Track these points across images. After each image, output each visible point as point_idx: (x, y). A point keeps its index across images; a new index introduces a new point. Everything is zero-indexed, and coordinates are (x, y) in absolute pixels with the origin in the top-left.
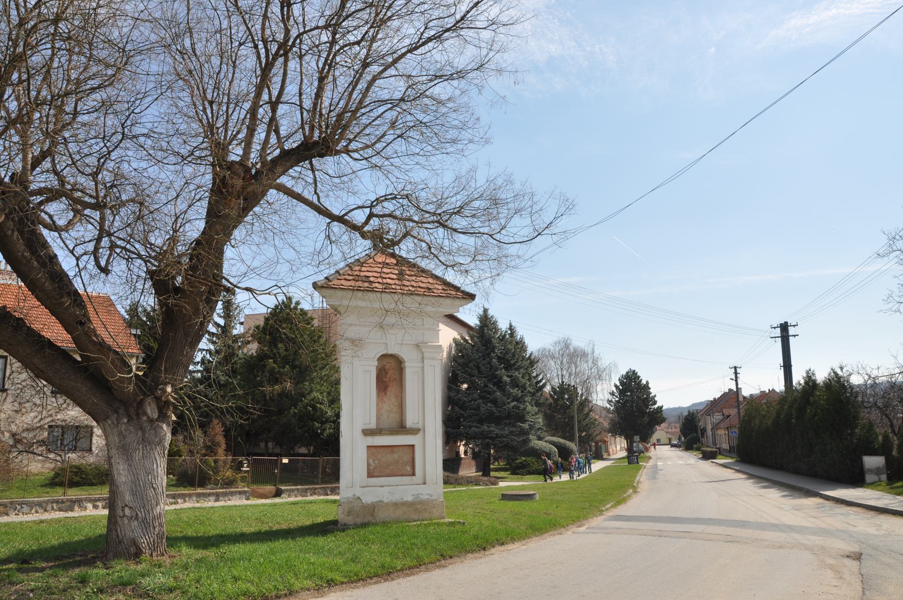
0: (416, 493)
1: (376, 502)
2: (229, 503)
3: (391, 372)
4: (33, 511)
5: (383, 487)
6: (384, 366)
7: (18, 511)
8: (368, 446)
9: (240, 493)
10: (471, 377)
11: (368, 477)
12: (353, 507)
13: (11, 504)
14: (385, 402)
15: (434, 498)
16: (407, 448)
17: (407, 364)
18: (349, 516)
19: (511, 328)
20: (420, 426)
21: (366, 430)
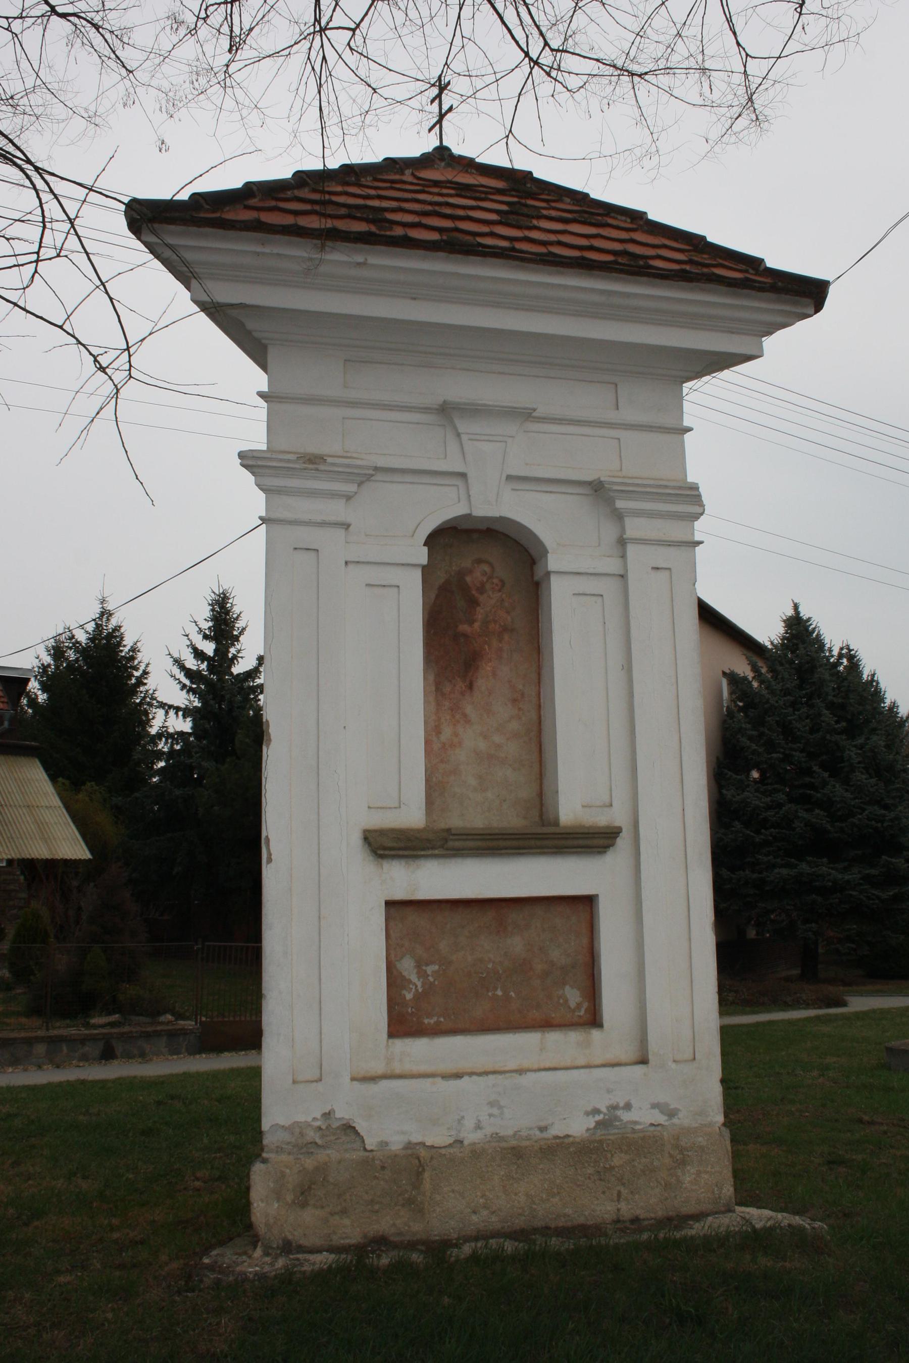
3: (489, 601)
5: (458, 1076)
6: (461, 574)
8: (389, 904)
10: (176, 1020)
11: (392, 1034)
12: (322, 1169)
14: (467, 720)
17: (554, 562)
18: (304, 1205)
19: (134, 649)
20: (618, 816)
21: (382, 832)
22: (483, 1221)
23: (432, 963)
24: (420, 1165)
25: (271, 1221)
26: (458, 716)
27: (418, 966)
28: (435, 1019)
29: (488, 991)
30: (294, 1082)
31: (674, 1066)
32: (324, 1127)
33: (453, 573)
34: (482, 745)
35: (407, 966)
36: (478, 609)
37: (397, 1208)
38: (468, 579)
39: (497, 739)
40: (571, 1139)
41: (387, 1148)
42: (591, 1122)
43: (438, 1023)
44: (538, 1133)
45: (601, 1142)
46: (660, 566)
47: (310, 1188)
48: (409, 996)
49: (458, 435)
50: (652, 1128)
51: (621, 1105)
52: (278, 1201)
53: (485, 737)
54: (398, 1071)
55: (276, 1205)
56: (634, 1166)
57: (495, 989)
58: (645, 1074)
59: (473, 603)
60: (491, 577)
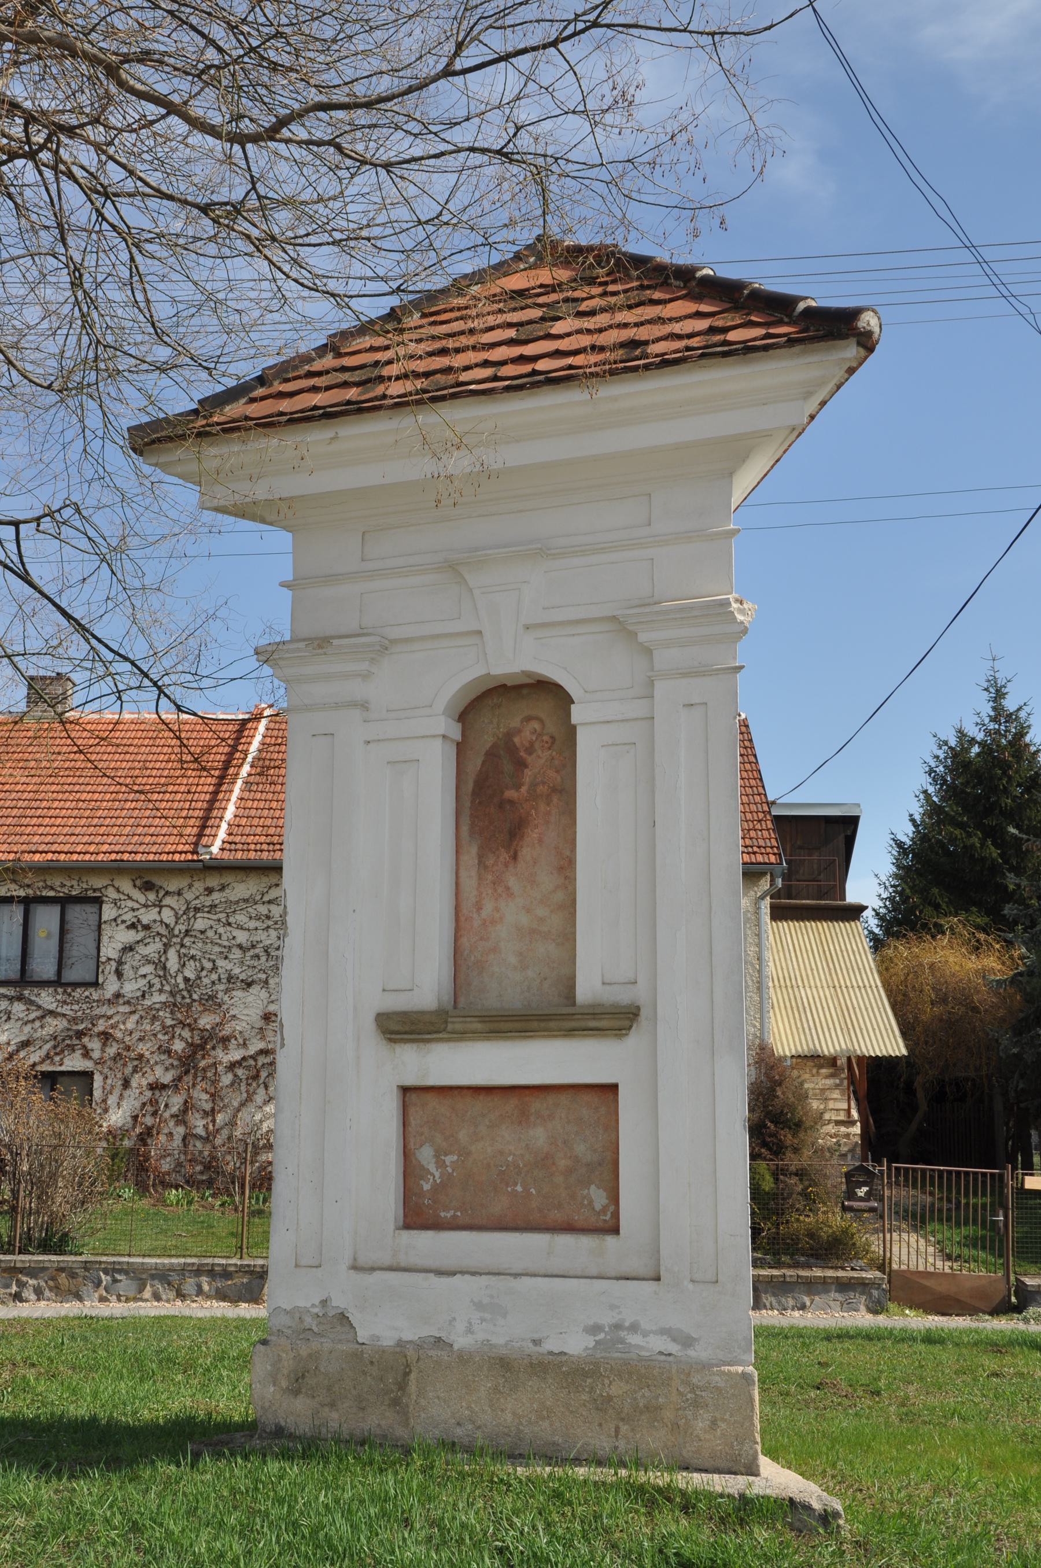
0: (607, 1319)
1: (419, 1345)
2: (796, 1318)
4: (147, 1293)
6: (509, 735)
7: (106, 1289)
9: (844, 1286)
11: (407, 1226)
12: (315, 1356)
13: (86, 1269)
14: (509, 892)
15: (699, 1353)
16: (586, 1097)
18: (296, 1392)
20: (639, 994)
22: (468, 1436)
23: (451, 1153)
24: (408, 1366)
25: (267, 1404)
26: (500, 890)
27: (438, 1155)
28: (452, 1212)
29: (507, 1185)
30: (297, 1266)
31: (691, 1286)
32: (321, 1314)
33: (500, 736)
34: (524, 920)
35: (425, 1155)
36: (526, 771)
37: (383, 1407)
38: (516, 740)
39: (541, 912)
40: (564, 1358)
41: (379, 1343)
42: (590, 1341)
43: (454, 1216)
44: (531, 1345)
45: (597, 1364)
46: (693, 702)
47: (303, 1377)
48: (427, 1187)
49: (471, 590)
50: (663, 1358)
51: (627, 1324)
52: (274, 1385)
53: (528, 911)
54: (403, 1264)
55: (272, 1389)
56: (635, 1399)
57: (516, 1184)
58: (655, 1293)
59: (521, 765)
60: (540, 735)
